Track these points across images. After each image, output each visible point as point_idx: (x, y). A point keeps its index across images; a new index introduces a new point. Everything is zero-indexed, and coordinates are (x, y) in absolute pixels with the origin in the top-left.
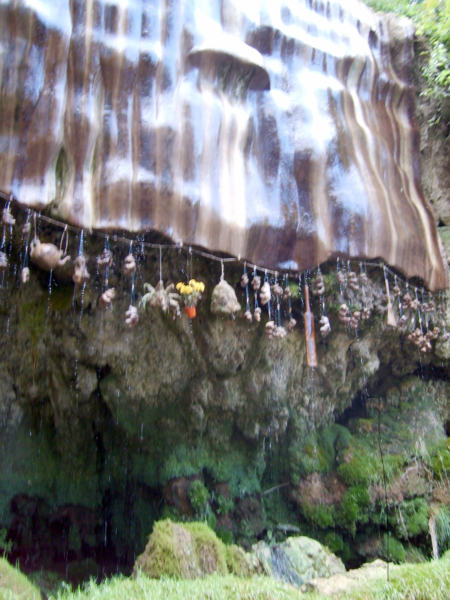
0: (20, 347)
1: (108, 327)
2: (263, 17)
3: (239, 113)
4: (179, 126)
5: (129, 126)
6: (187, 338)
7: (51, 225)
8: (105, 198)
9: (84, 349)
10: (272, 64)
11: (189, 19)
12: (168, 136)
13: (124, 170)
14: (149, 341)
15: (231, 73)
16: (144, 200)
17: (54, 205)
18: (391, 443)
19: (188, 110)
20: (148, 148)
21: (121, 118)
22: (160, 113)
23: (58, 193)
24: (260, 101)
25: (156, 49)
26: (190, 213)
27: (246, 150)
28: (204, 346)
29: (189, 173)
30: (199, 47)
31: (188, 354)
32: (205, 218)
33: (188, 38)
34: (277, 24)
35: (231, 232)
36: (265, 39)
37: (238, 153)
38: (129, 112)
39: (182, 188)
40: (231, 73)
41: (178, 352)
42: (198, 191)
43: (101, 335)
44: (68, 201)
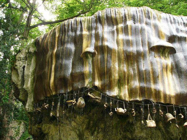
0: (114, 136)
1: (138, 128)
2: (171, 32)
3: (169, 61)
4: (150, 69)
5: (136, 72)
6: (162, 130)
7: (120, 102)
8: (132, 92)
9: (132, 135)
10: (176, 45)
11: (149, 38)
12: (147, 72)
13: (136, 84)
14: (151, 132)
15: (160, 50)
16: (143, 91)
17: (118, 95)
18: (121, 135)
19: (152, 63)
20: (143, 76)
21: (134, 70)
22: (144, 66)
23: (119, 92)
24: (174, 57)
25: (141, 49)
26: (157, 93)
27: (172, 72)
28: (168, 132)
29: (155, 82)
30: (152, 46)
31: (163, 135)
32: (162, 95)
33: (149, 44)
34: (175, 33)
35: (170, 97)
36: (172, 39)
37: (169, 73)
38: (136, 67)
39: (153, 86)
40: (160, 50)
41: (160, 134)
42: (160, 87)
43: (137, 131)
44: (122, 94)
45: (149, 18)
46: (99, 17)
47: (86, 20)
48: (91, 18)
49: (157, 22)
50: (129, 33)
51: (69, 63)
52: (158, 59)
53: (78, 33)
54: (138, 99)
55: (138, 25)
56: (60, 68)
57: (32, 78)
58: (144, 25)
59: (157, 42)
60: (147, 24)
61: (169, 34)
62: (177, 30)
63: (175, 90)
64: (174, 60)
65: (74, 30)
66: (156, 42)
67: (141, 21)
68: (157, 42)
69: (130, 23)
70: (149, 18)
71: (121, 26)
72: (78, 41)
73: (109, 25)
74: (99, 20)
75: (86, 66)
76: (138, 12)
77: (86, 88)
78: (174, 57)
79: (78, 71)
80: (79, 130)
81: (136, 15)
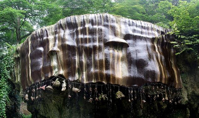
3: (120, 54)
8: (89, 77)
19: (106, 55)
25: (97, 44)
34: (131, 32)
36: (127, 37)
45: (107, 21)
46: (61, 25)
47: (50, 28)
48: (54, 26)
49: (115, 24)
50: (87, 32)
51: (40, 60)
52: (111, 51)
53: (45, 38)
54: (93, 81)
55: (96, 27)
56: (34, 65)
57: (20, 74)
58: (103, 28)
59: (113, 38)
60: (105, 26)
61: (124, 33)
62: (134, 31)
63: (123, 73)
64: (126, 52)
65: (42, 37)
66: (111, 38)
67: (99, 24)
68: (113, 38)
69: (87, 26)
70: (107, 21)
71: (80, 28)
72: (45, 43)
73: (70, 28)
74: (61, 26)
75: (52, 60)
76: (96, 18)
77: (54, 76)
78: (126, 50)
79: (48, 65)
80: (58, 105)
81: (94, 19)
